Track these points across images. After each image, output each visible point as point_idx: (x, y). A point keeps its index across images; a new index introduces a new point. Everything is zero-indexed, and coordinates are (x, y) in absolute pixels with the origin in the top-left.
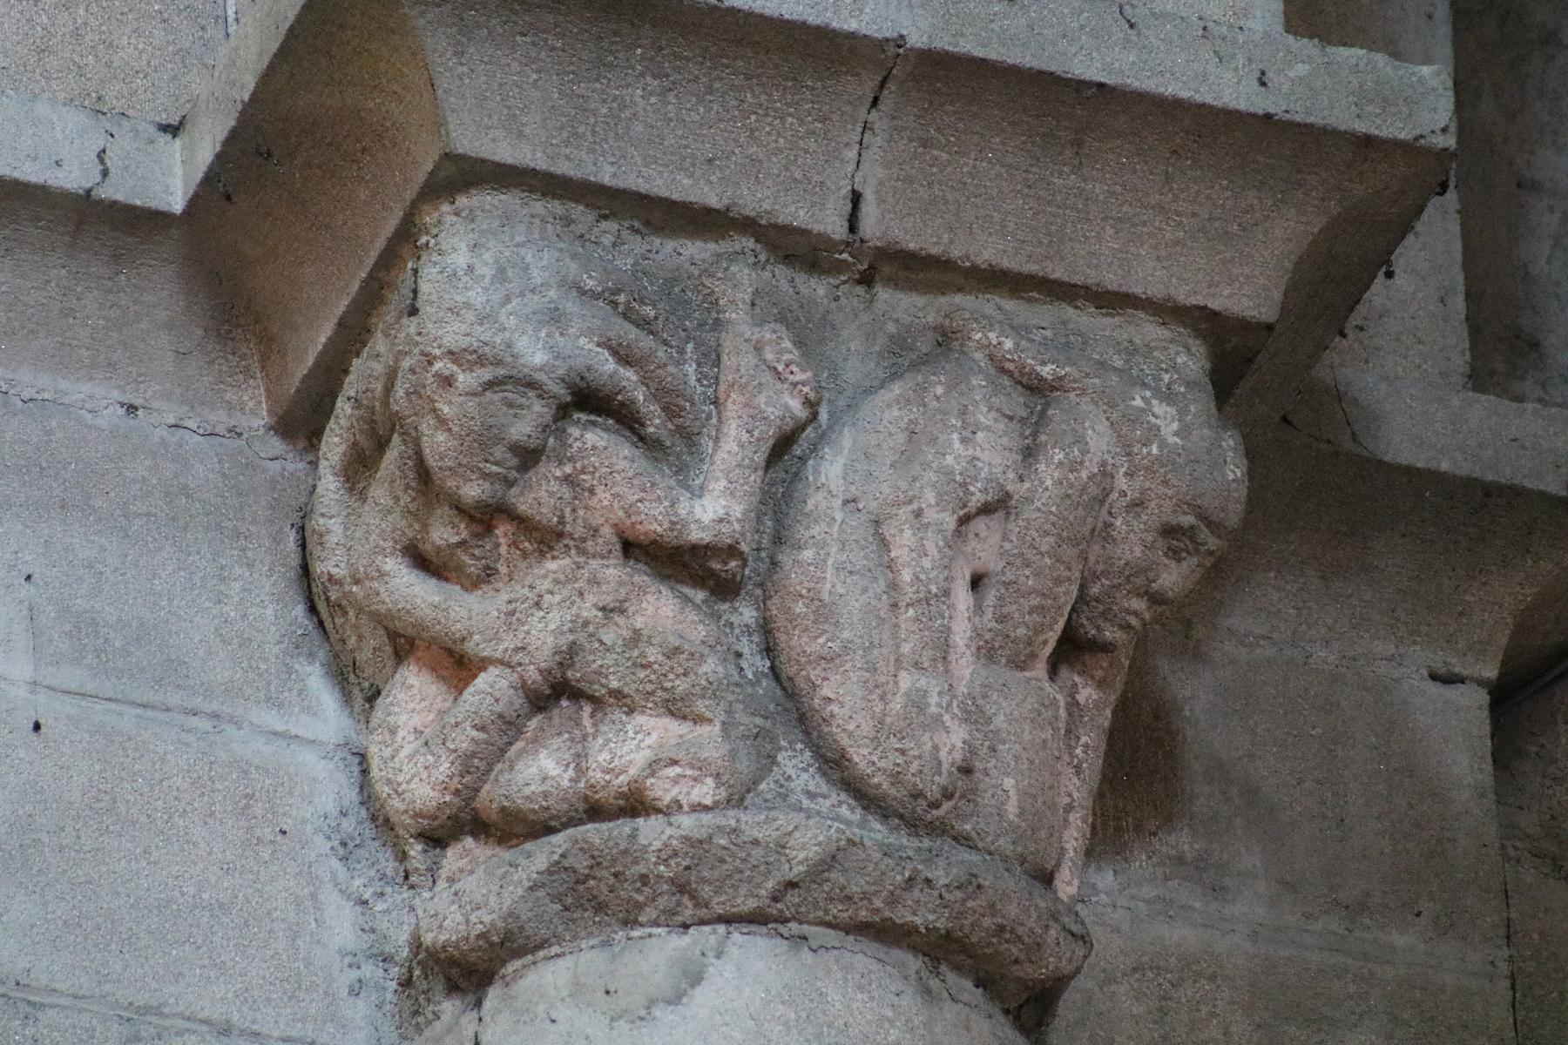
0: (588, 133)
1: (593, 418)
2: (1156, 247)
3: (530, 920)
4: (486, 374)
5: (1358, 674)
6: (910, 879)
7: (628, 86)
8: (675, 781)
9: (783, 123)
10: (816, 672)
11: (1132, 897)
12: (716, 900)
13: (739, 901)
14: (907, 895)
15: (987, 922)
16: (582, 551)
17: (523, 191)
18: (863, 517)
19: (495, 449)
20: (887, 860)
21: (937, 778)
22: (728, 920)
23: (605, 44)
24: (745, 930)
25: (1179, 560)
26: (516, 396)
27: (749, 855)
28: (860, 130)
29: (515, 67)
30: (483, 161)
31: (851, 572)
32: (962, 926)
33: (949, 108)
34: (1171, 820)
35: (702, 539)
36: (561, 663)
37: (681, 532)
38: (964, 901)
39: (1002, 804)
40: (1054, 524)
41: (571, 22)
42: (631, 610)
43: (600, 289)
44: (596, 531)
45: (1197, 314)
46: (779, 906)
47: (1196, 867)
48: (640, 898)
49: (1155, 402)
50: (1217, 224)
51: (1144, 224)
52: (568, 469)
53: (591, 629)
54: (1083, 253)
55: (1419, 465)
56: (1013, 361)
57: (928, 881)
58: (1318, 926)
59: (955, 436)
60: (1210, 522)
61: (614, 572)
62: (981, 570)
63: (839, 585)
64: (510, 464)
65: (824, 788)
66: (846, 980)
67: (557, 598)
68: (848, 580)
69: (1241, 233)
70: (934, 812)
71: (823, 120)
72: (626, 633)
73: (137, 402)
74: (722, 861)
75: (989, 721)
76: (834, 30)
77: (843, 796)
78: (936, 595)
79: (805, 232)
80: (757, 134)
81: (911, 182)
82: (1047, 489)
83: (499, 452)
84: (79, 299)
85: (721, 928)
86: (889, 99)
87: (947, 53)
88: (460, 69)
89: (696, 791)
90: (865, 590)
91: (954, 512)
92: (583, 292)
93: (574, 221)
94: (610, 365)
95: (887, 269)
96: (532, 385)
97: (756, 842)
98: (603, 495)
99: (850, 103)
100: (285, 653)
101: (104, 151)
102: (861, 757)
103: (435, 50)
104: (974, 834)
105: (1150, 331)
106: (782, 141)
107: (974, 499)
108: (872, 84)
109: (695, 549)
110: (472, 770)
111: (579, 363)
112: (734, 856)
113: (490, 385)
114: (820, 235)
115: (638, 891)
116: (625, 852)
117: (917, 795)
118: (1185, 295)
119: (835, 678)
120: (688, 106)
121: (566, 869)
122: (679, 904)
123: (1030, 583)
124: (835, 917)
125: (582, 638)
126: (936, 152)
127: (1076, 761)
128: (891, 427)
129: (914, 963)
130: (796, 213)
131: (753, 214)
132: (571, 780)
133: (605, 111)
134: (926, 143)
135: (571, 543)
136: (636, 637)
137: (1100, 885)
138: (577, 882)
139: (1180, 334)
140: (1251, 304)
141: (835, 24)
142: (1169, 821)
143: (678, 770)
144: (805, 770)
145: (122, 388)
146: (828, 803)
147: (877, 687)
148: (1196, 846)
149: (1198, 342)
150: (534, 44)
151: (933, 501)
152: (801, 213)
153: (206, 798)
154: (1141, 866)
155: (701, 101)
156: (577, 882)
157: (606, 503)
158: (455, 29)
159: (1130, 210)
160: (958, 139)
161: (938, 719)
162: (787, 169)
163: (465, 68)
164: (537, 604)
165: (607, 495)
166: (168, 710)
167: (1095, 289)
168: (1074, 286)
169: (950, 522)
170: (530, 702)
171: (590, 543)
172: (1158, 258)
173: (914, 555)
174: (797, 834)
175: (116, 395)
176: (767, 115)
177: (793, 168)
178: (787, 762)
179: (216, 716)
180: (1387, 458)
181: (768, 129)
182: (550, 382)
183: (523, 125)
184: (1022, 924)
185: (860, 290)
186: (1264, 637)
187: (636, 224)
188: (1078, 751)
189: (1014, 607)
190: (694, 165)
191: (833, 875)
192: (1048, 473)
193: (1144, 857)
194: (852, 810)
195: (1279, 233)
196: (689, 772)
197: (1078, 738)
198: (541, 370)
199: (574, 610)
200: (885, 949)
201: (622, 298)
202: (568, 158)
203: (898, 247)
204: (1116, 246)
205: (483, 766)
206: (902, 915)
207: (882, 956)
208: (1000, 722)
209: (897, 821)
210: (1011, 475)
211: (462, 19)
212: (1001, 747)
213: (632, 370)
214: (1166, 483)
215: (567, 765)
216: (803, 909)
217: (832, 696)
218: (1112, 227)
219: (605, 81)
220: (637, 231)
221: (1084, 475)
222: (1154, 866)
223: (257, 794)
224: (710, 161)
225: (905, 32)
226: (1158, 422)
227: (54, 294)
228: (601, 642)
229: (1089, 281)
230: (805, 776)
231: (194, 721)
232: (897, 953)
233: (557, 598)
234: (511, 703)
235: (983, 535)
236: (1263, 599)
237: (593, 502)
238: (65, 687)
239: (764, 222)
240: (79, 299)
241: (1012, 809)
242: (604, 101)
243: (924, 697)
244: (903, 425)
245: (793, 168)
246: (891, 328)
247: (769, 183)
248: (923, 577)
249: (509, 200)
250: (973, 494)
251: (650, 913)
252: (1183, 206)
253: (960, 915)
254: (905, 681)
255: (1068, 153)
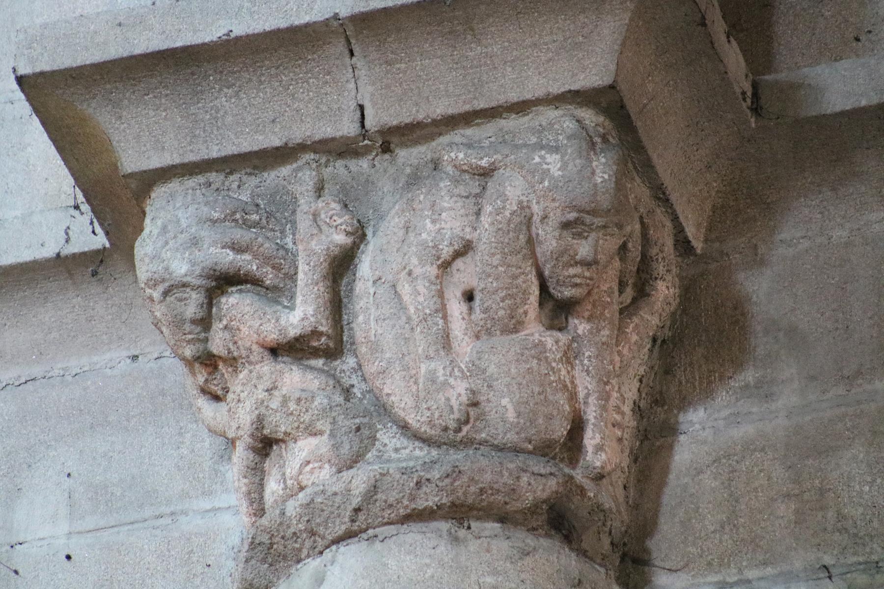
0: (202, 133)
1: (239, 287)
2: (537, 68)
3: (254, 579)
4: (161, 288)
5: (863, 237)
6: (417, 483)
7: (216, 98)
8: (312, 472)
9: (308, 83)
10: (379, 382)
11: (716, 420)
12: (328, 532)
13: (337, 529)
14: (420, 492)
15: (473, 489)
16: (250, 363)
17: (179, 178)
18: (387, 285)
19: (185, 326)
20: (405, 477)
21: (452, 416)
22: (337, 541)
23: (191, 82)
24: (345, 544)
25: (586, 238)
26: (181, 294)
27: (334, 502)
28: (351, 70)
29: (152, 113)
30: (145, 172)
31: (384, 320)
32: (458, 498)
33: (389, 40)
34: (742, 365)
35: (296, 333)
36: (257, 428)
37: (285, 334)
38: (452, 484)
39: (503, 414)
40: (496, 248)
41: (166, 78)
42: (280, 385)
43: (223, 216)
44: (250, 349)
45: (569, 95)
46: (357, 524)
47: (756, 387)
48: (297, 546)
49: (548, 156)
50: (570, 41)
51: (528, 57)
52: (225, 322)
53: (265, 404)
54: (495, 88)
55: (847, 108)
56: (465, 164)
57: (428, 480)
58: (829, 395)
59: (428, 221)
60: (587, 211)
61: (267, 367)
62: (468, 288)
63: (379, 329)
64: (196, 331)
65: (405, 442)
66: (400, 551)
67: (246, 393)
68: (384, 324)
69: (585, 40)
70: (459, 434)
71: (329, 73)
72: (280, 399)
73: (136, 353)
74: (323, 511)
75: (484, 371)
76: (297, 26)
77: (417, 443)
78: (430, 314)
79: (333, 139)
80: (296, 95)
81: (390, 87)
82: (486, 230)
83: (188, 327)
84: (93, 309)
85: (334, 548)
86: (357, 50)
87: (363, 13)
88: (122, 127)
89: (322, 474)
90: (394, 326)
91: (432, 264)
92: (214, 222)
93: (213, 182)
94: (230, 256)
95: (395, 140)
96: (184, 285)
97: (335, 494)
98: (245, 330)
99: (338, 59)
100: (215, 463)
101: (68, 228)
102: (412, 420)
103: (105, 122)
104: (488, 438)
105: (551, 114)
106: (311, 94)
107: (444, 252)
108: (341, 44)
109: (297, 339)
110: (254, 500)
111: (208, 263)
112: (326, 505)
113: (166, 294)
114: (342, 137)
115: (296, 542)
116: (281, 524)
117: (446, 429)
118: (556, 89)
119: (388, 381)
120: (253, 96)
121: (259, 544)
122: (315, 542)
123: (494, 285)
124: (389, 519)
125: (263, 410)
126: (398, 66)
127: (586, 367)
128: (394, 229)
129: (444, 526)
130: (326, 131)
131: (301, 141)
132: (283, 489)
133: (208, 117)
134: (388, 63)
135: (244, 361)
136: (285, 400)
137: (695, 420)
138: (269, 549)
139: (569, 110)
140: (598, 78)
141: (297, 23)
142: (739, 365)
143: (311, 466)
144: (393, 437)
145: (128, 349)
146: (407, 451)
147: (411, 377)
148: (757, 375)
149: (584, 109)
150: (155, 97)
151: (417, 263)
152: (329, 129)
153: (165, 562)
154: (722, 399)
155: (259, 90)
156: (269, 549)
157: (247, 333)
158: (110, 106)
159: (517, 53)
160: (406, 53)
161: (445, 383)
162: (318, 108)
163: (125, 125)
164: (239, 401)
165: (246, 328)
166: (146, 520)
167: (505, 105)
168: (493, 108)
169: (433, 271)
170: (258, 454)
171: (251, 357)
172: (540, 74)
173: (413, 297)
174: (354, 481)
175: (125, 353)
176: (297, 83)
177: (321, 106)
178: (383, 436)
179: (172, 514)
180: (829, 112)
181: (301, 90)
182: (194, 280)
183: (164, 143)
184: (497, 483)
185: (387, 156)
186: (803, 238)
187: (248, 170)
188: (586, 362)
189: (490, 302)
190: (264, 126)
191: (379, 496)
192: (485, 220)
193: (724, 394)
194: (421, 449)
195: (606, 32)
196: (316, 465)
197: (584, 354)
198: (186, 275)
199: (255, 397)
200: (426, 524)
201: (238, 216)
202: (192, 151)
203: (387, 127)
204: (514, 76)
205: (256, 496)
206: (421, 504)
207: (424, 529)
208: (492, 369)
209: (445, 447)
210: (468, 230)
211: (110, 100)
212: (495, 383)
213: (247, 254)
214: (554, 200)
215: (280, 482)
216: (370, 521)
217: (390, 392)
218: (509, 67)
219: (203, 101)
220: (250, 174)
221: (507, 213)
222: (730, 396)
223: (195, 549)
224: (273, 121)
225: (337, 11)
226: (550, 166)
227: (79, 312)
228: (272, 409)
229: (500, 102)
230: (395, 440)
231: (161, 521)
232: (435, 525)
233: (246, 393)
234: (248, 458)
235: (462, 269)
236: (800, 215)
237: (242, 335)
238: (87, 529)
239: (309, 143)
240: (93, 309)
241: (511, 415)
242: (207, 112)
243: (434, 373)
244: (401, 226)
245: (321, 106)
246: (408, 170)
247: (308, 120)
248: (420, 307)
249: (174, 185)
250: (442, 250)
251: (305, 552)
252: (547, 39)
253: (453, 491)
254: (423, 368)
255: (469, 37)
